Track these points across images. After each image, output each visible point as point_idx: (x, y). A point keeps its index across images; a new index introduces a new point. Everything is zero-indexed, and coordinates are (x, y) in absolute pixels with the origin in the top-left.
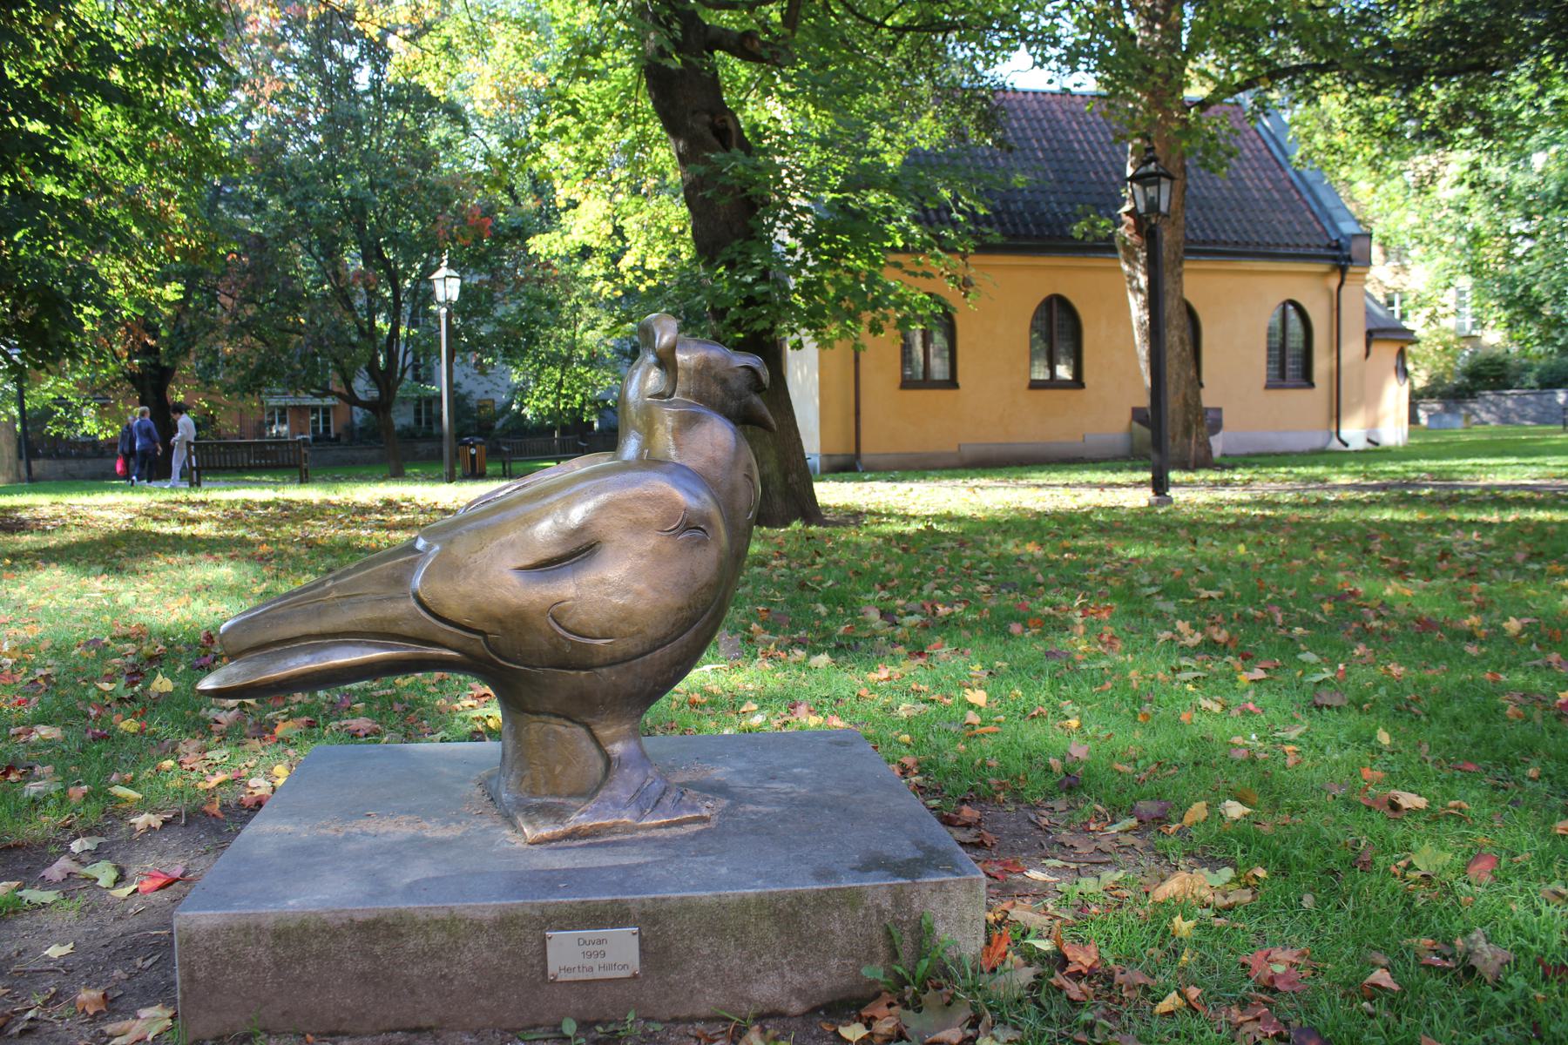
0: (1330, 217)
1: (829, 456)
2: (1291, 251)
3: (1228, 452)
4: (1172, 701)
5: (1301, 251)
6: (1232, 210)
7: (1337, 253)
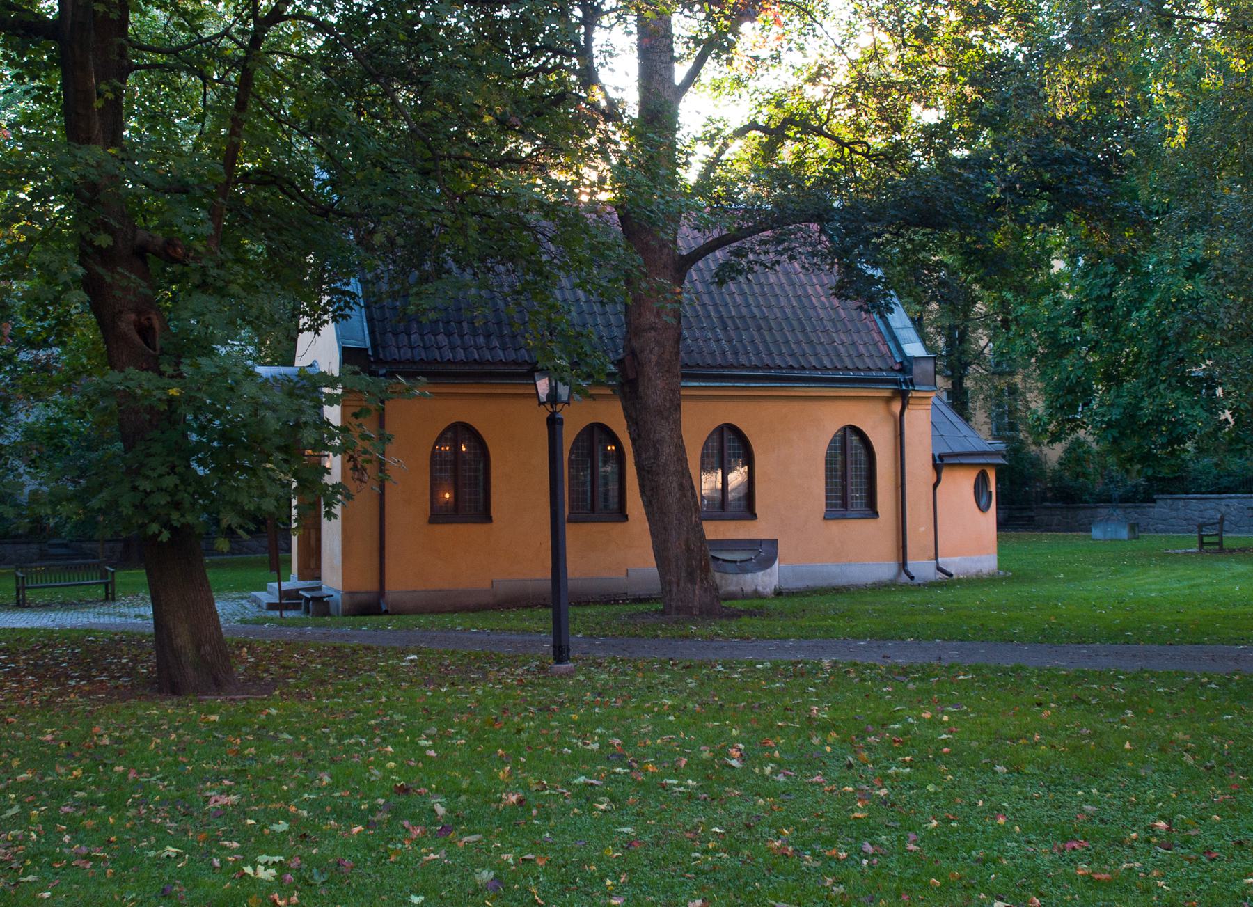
0: (895, 339)
2: (851, 375)
4: (601, 859)
6: (793, 330)
7: (900, 377)
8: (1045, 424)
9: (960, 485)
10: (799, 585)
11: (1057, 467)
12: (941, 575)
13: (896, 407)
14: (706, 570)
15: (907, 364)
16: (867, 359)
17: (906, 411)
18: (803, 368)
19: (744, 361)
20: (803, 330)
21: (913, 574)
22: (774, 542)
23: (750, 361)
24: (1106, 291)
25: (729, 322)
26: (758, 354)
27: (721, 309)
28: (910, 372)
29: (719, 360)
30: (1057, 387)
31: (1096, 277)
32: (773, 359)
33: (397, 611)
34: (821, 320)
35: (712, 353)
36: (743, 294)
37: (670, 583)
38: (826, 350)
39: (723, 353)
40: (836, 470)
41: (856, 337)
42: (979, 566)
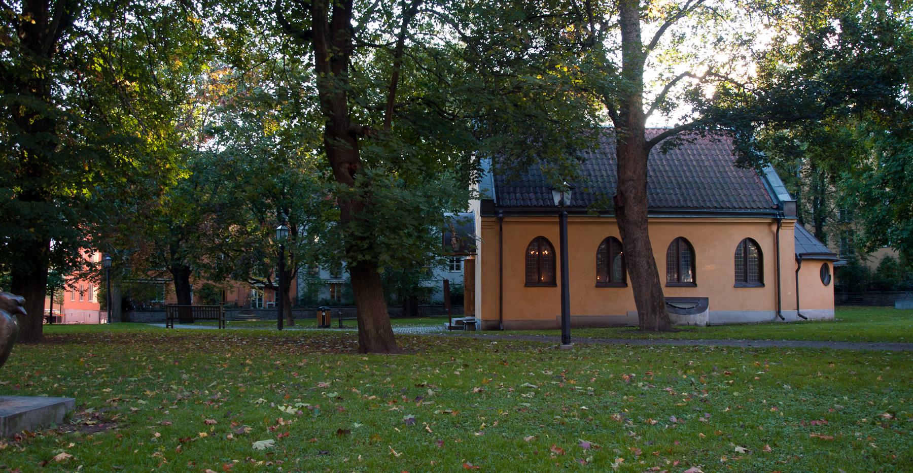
0: (774, 192)
1: (486, 321)
3: (712, 322)
5: (755, 211)
7: (776, 212)
8: (864, 242)
9: (812, 271)
10: (720, 322)
11: (876, 272)
12: (801, 319)
13: (774, 228)
14: (662, 307)
15: (780, 205)
16: (758, 203)
17: (780, 230)
18: (722, 208)
19: (689, 204)
20: (723, 189)
21: (784, 317)
22: (706, 299)
23: (693, 204)
24: (900, 168)
25: (683, 186)
26: (697, 201)
27: (678, 179)
28: (782, 209)
29: (676, 204)
30: (871, 222)
31: (893, 161)
32: (706, 203)
33: (509, 328)
34: (733, 183)
35: (673, 201)
36: (691, 171)
37: (643, 314)
38: (735, 198)
39: (679, 201)
40: (741, 261)
41: (752, 192)
42: (823, 315)
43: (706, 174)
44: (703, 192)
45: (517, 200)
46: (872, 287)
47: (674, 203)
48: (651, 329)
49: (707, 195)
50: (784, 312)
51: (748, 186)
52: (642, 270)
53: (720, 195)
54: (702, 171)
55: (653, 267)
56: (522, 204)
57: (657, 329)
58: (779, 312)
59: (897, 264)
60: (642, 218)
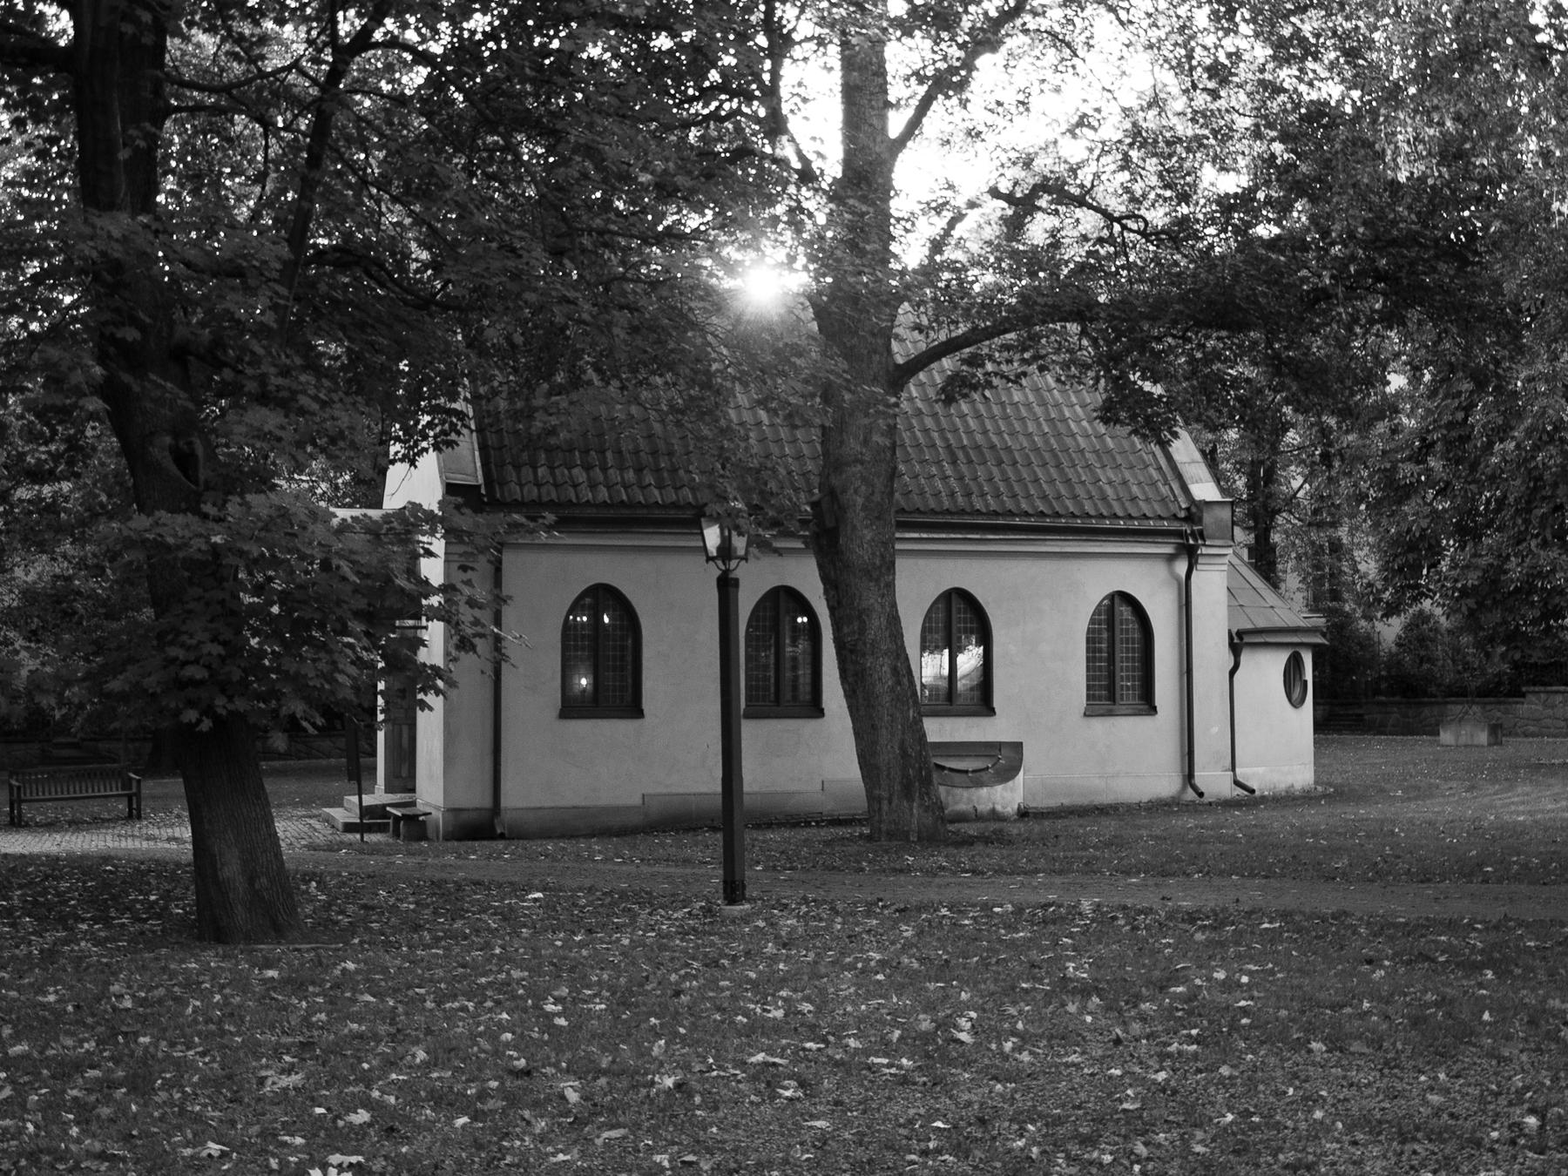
7: (1186, 528)
9: (1266, 669)
11: (1394, 649)
12: (1240, 791)
13: (1181, 567)
15: (1195, 512)
17: (1194, 573)
18: (1057, 515)
19: (979, 505)
20: (1058, 466)
21: (1202, 789)
22: (1018, 747)
23: (987, 505)
25: (960, 455)
26: (998, 496)
27: (949, 436)
28: (1200, 521)
29: (947, 504)
30: (1395, 542)
32: (1018, 504)
33: (516, 834)
36: (979, 416)
37: (879, 800)
38: (1088, 492)
39: (952, 494)
40: (1100, 651)
41: (1127, 475)
43: (1017, 426)
44: (1010, 471)
45: (539, 485)
46: (1384, 686)
47: (940, 502)
48: (899, 836)
49: (1020, 480)
50: (1201, 777)
51: (1119, 459)
52: (879, 688)
53: (1052, 482)
54: (1006, 418)
55: (905, 680)
56: (554, 496)
57: (913, 838)
58: (1189, 777)
59: (1443, 630)
60: (882, 557)
